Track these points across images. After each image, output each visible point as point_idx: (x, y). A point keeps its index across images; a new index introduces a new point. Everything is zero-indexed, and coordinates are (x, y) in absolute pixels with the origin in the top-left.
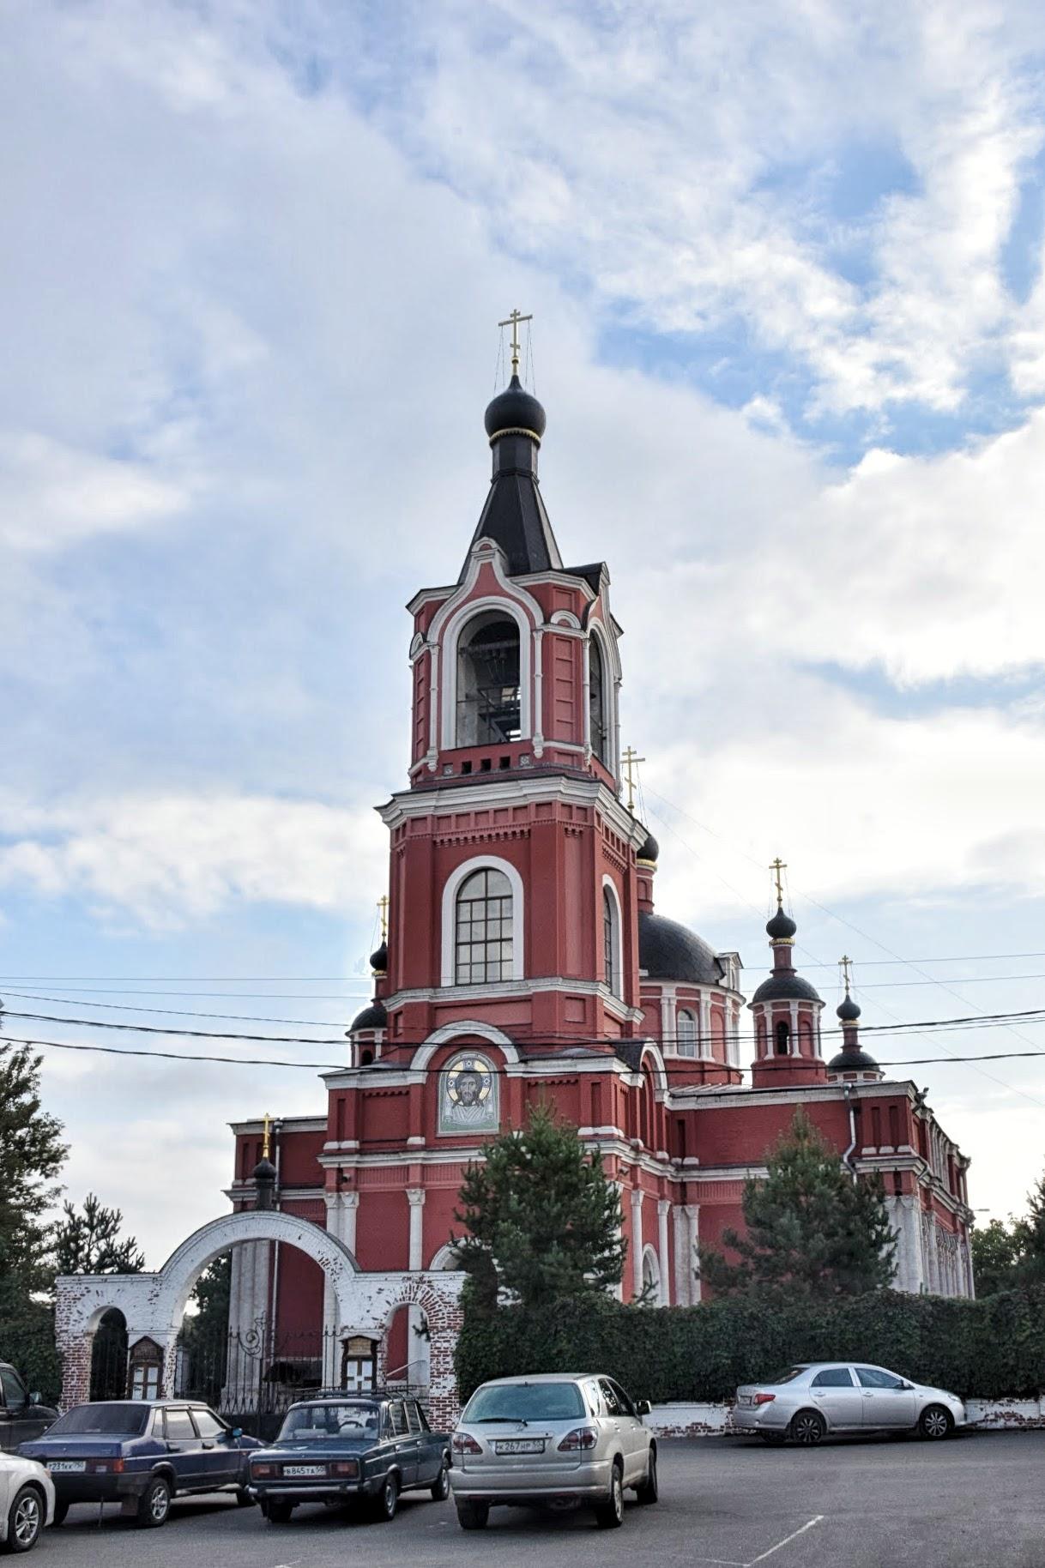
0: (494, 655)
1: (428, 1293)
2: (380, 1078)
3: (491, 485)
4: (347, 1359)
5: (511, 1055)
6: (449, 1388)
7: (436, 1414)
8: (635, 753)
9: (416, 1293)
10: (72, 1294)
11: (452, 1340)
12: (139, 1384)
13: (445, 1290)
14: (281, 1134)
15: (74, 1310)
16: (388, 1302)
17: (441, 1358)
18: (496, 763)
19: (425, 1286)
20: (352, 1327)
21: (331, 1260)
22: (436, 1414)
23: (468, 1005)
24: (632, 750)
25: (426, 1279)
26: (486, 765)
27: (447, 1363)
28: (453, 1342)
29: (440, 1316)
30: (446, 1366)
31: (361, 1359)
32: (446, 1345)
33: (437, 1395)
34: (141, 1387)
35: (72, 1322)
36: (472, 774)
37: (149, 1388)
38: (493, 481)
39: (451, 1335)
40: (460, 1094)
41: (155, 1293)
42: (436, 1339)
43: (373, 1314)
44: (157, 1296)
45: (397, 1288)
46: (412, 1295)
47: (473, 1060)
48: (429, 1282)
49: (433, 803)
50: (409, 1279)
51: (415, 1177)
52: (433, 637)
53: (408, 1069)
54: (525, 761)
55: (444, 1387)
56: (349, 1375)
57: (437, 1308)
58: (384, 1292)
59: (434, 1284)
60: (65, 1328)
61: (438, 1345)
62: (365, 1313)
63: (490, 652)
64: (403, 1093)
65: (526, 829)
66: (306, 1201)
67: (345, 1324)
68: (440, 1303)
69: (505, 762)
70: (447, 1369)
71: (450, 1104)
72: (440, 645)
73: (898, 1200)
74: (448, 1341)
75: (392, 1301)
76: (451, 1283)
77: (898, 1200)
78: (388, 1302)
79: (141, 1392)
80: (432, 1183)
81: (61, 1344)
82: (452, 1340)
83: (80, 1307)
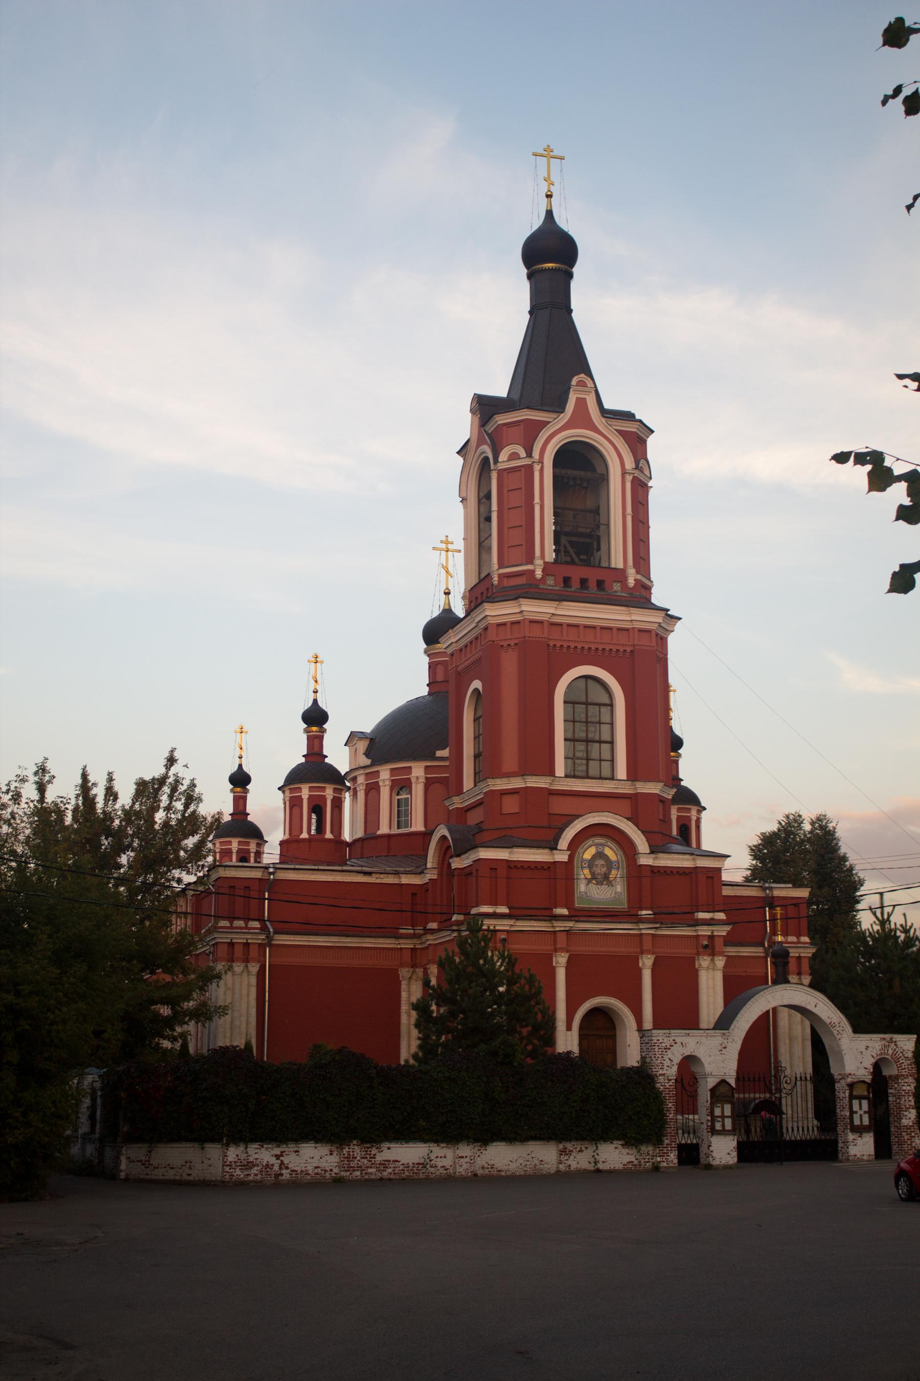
0: (578, 482)
1: (895, 1050)
4: (852, 1097)
5: (642, 844)
6: (912, 1119)
10: (664, 1045)
12: (719, 1117)
14: (274, 879)
15: (666, 1057)
16: (872, 1056)
17: (906, 1097)
18: (592, 584)
19: (893, 1045)
20: (854, 1074)
21: (837, 1024)
22: (906, 1137)
23: (572, 795)
25: (894, 1040)
26: (584, 582)
29: (903, 1067)
30: (910, 1103)
31: (860, 1098)
32: (908, 1088)
33: (906, 1124)
34: (720, 1119)
35: (665, 1068)
36: (573, 589)
37: (726, 1120)
39: (911, 1081)
40: (593, 874)
41: (724, 1045)
42: (902, 1084)
43: (865, 1065)
44: (725, 1048)
45: (877, 1045)
46: (886, 1051)
48: (895, 1042)
49: (553, 611)
50: (884, 1039)
51: (562, 940)
52: (536, 454)
53: (556, 849)
54: (617, 587)
55: (910, 1118)
56: (854, 1110)
57: (901, 1061)
58: (869, 1049)
59: (898, 1043)
60: (661, 1072)
61: (904, 1088)
62: (859, 1065)
63: (575, 479)
64: (553, 866)
65: (629, 649)
66: (293, 946)
67: (849, 1072)
68: (902, 1058)
71: (584, 882)
72: (541, 461)
74: (909, 1085)
75: (875, 1056)
76: (907, 1043)
78: (872, 1056)
79: (721, 1123)
80: (514, 946)
81: (659, 1085)
83: (670, 1056)
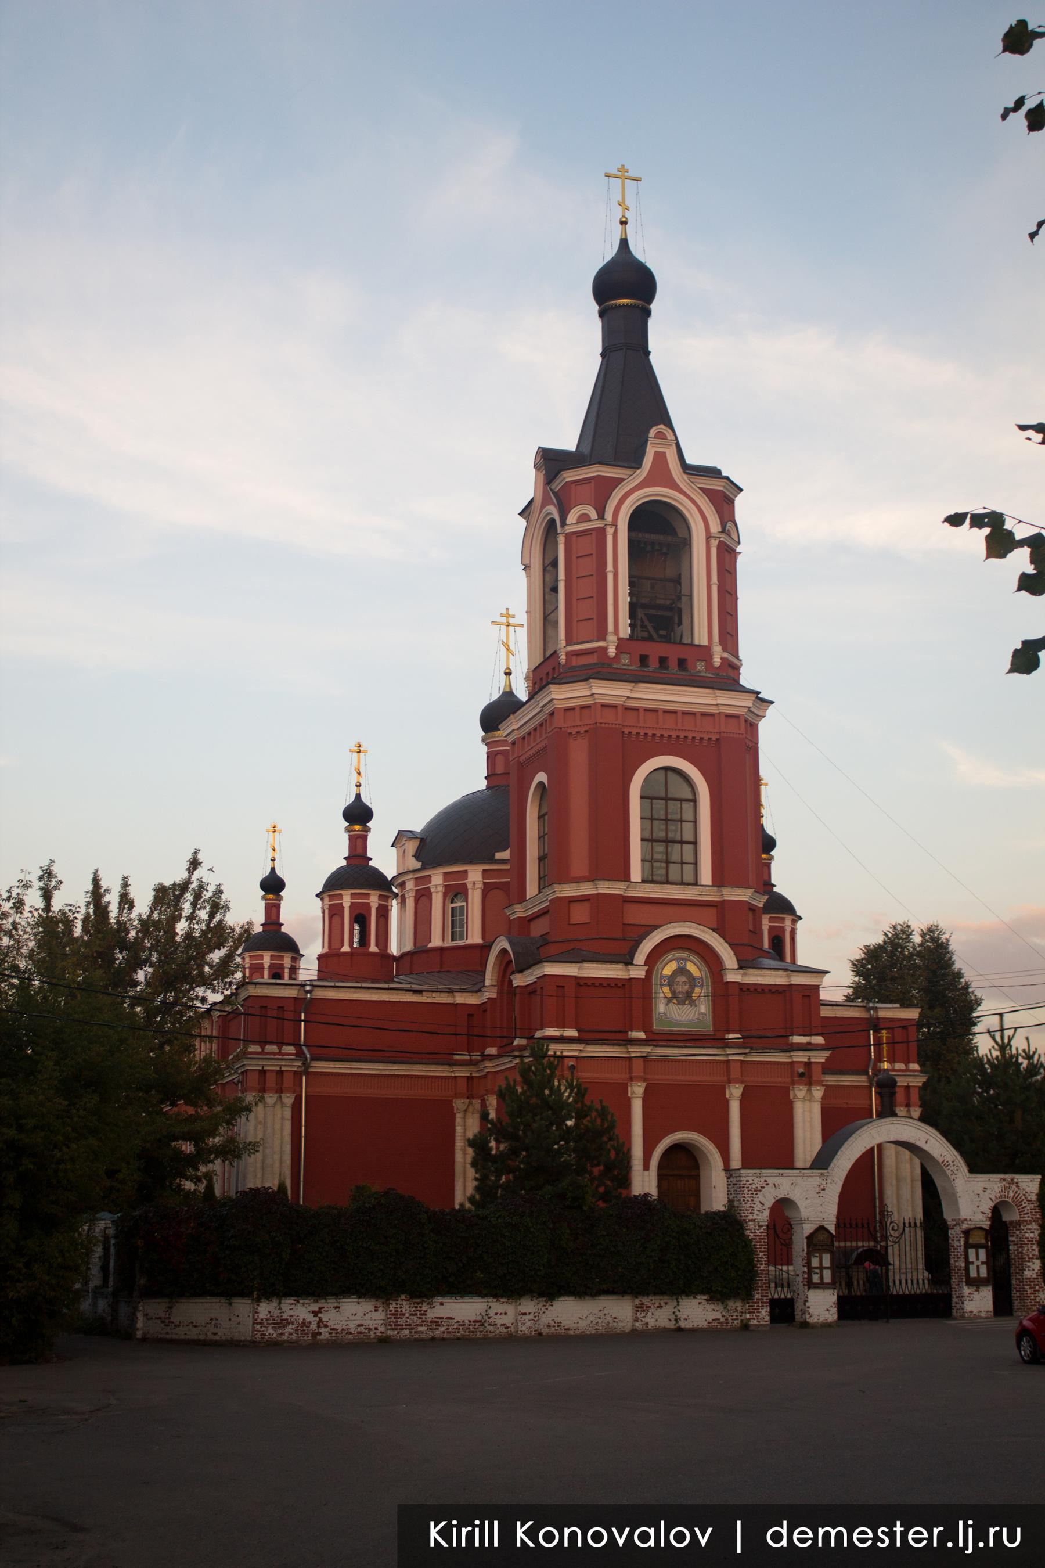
1: (1016, 1192)
2: (597, 969)
3: (600, 359)
4: (968, 1246)
5: (729, 958)
6: (1036, 1271)
7: (1029, 1291)
8: (513, 617)
9: (1008, 1192)
11: (1035, 1231)
12: (816, 1268)
13: (1028, 1190)
14: (311, 998)
15: (756, 1200)
16: (991, 1199)
17: (1029, 1246)
18: (673, 664)
20: (970, 1220)
21: (950, 1162)
22: (1029, 1291)
24: (504, 612)
25: (1015, 1180)
26: (663, 661)
27: (1033, 1250)
28: (1037, 1233)
30: (1034, 1253)
31: (977, 1247)
32: (1032, 1235)
33: (1029, 1276)
36: (651, 669)
38: (603, 355)
40: (673, 992)
41: (822, 1187)
43: (982, 1209)
44: (824, 1190)
45: (996, 1187)
46: (1006, 1194)
47: (685, 960)
48: (1017, 1183)
49: (628, 694)
50: (1004, 1180)
51: (638, 1067)
53: (631, 964)
54: (700, 666)
55: (1033, 1270)
56: (970, 1260)
57: (1024, 1205)
58: (988, 1191)
59: (1020, 1184)
60: (751, 1217)
61: (1027, 1235)
62: (975, 1209)
63: (653, 544)
64: (628, 983)
65: (714, 737)
66: (332, 1074)
67: (964, 1217)
68: (1025, 1201)
69: (682, 663)
70: (1034, 1255)
73: (809, 1090)
74: (1033, 1232)
75: (994, 1198)
77: (809, 1090)
78: (991, 1199)
79: (819, 1275)
81: (748, 1231)
82: (1035, 1231)
83: (761, 1198)
